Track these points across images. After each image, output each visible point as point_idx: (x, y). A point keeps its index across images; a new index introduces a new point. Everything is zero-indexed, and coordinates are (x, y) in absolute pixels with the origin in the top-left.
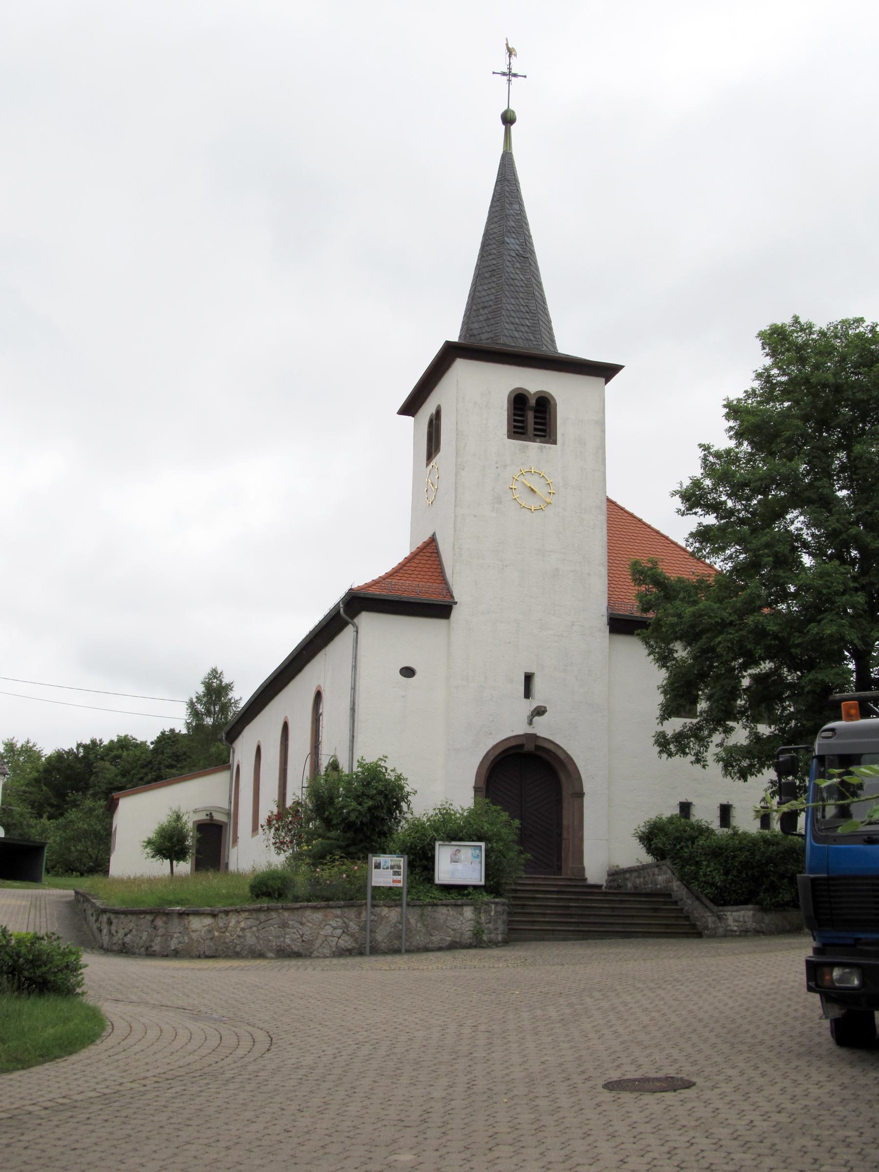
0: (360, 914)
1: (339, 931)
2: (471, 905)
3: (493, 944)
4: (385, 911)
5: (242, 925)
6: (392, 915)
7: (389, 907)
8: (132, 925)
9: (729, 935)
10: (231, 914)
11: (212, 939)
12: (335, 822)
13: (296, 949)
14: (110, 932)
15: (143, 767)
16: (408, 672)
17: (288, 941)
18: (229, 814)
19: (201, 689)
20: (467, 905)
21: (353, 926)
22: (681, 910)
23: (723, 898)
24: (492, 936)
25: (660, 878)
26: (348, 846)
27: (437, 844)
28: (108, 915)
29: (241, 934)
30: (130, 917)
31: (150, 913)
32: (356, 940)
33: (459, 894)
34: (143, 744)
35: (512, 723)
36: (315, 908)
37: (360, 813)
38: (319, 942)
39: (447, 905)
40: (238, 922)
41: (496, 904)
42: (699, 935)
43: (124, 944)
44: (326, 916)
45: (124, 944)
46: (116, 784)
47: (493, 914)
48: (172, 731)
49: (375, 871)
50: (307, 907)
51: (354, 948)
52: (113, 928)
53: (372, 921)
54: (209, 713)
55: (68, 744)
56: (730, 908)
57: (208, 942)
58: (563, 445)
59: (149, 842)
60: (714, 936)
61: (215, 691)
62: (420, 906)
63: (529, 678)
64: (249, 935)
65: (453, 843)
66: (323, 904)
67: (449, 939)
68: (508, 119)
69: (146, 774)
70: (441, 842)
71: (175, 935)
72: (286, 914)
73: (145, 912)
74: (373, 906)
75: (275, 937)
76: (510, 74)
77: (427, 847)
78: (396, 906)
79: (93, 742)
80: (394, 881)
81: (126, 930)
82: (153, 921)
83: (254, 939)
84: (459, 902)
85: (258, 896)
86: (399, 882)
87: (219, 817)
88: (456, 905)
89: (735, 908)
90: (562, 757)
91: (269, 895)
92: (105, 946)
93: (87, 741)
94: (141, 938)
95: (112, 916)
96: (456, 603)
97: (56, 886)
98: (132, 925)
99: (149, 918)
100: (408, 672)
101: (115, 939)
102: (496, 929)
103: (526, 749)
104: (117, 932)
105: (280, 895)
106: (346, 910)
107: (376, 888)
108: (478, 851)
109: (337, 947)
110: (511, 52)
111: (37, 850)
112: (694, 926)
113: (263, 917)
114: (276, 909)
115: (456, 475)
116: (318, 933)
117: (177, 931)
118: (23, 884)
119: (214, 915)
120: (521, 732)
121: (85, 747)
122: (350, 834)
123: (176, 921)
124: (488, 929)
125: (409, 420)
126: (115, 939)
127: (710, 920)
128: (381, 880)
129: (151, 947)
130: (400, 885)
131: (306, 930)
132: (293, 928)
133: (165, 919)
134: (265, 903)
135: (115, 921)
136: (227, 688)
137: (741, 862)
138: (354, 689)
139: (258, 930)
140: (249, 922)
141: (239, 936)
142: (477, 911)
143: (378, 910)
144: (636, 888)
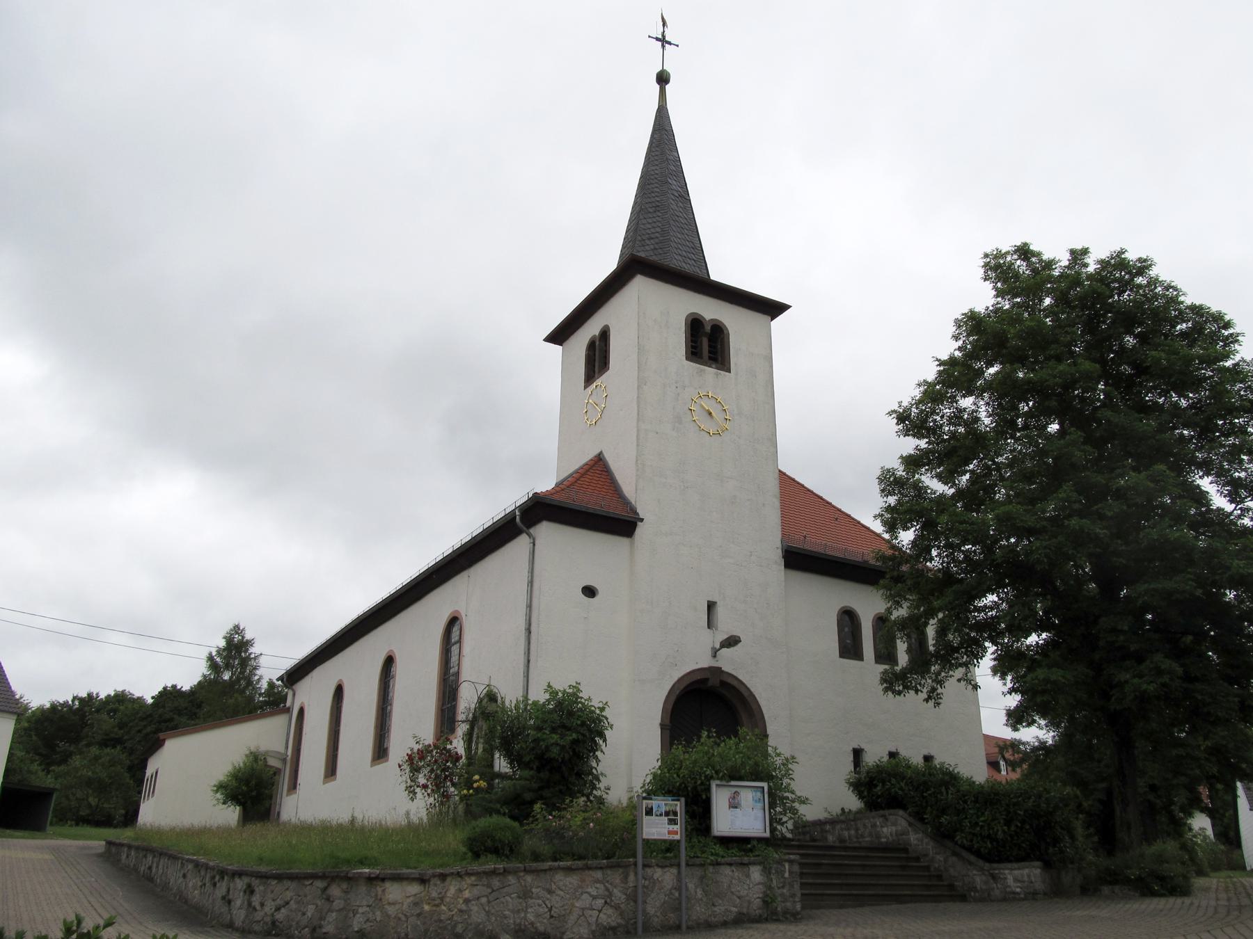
0: (626, 877)
1: (600, 902)
2: (760, 864)
3: (792, 917)
4: (658, 873)
5: (467, 894)
6: (666, 877)
7: (662, 867)
8: (289, 894)
9: (1009, 898)
10: (449, 879)
11: (419, 915)
12: (527, 759)
13: (541, 928)
14: (250, 904)
15: (142, 719)
16: (590, 592)
17: (531, 917)
18: (284, 761)
19: (222, 643)
20: (754, 864)
21: (619, 896)
22: (927, 868)
23: (998, 853)
24: (788, 904)
25: (885, 830)
26: (541, 788)
27: (714, 784)
28: (246, 880)
29: (464, 907)
30: (287, 883)
31: (323, 877)
32: (621, 914)
33: (740, 850)
34: (140, 700)
35: (696, 656)
36: (569, 870)
37: (563, 747)
38: (573, 918)
39: (731, 864)
40: (460, 891)
41: (791, 862)
42: (963, 898)
43: (274, 923)
44: (583, 881)
45: (274, 923)
46: (112, 735)
47: (787, 875)
48: (174, 687)
49: (646, 819)
50: (559, 868)
51: (619, 925)
52: (256, 900)
53: (644, 886)
54: (228, 666)
55: (64, 696)
56: (1009, 865)
57: (412, 920)
58: (737, 374)
59: (221, 787)
60: (986, 898)
61: (236, 650)
62: (702, 865)
63: (711, 606)
64: (475, 908)
65: (733, 783)
66: (580, 863)
67: (734, 909)
68: (663, 79)
69: (145, 726)
70: (718, 782)
71: (360, 910)
72: (529, 878)
73: (314, 877)
74: (645, 866)
75: (513, 911)
76: (663, 41)
77: (699, 788)
78: (671, 866)
79: (90, 695)
80: (670, 833)
81: (279, 902)
82: (325, 889)
83: (483, 914)
84: (746, 860)
85: (477, 855)
86: (676, 833)
87: (273, 762)
88: (742, 864)
89: (1015, 865)
90: (746, 694)
91: (496, 851)
92: (238, 923)
93: (84, 695)
94: (304, 914)
95: (255, 882)
96: (642, 520)
97: (75, 837)
98: (289, 894)
99: (320, 884)
100: (590, 592)
101: (258, 916)
102: (793, 896)
103: (710, 683)
104: (262, 905)
105: (511, 850)
106: (609, 872)
107: (647, 842)
108: (759, 794)
109: (597, 925)
110: (664, 24)
111: (43, 796)
112: (951, 887)
113: (496, 882)
114: (514, 872)
115: (639, 387)
116: (573, 905)
117: (365, 903)
118: (26, 833)
119: (423, 881)
120: (705, 665)
121: (81, 700)
122: (545, 775)
123: (363, 889)
124: (782, 895)
125: (558, 348)
126: (258, 916)
127: (979, 880)
128: (654, 830)
129: (321, 927)
130: (677, 837)
131: (555, 901)
132: (539, 898)
133: (345, 886)
134: (490, 863)
135: (259, 889)
136: (249, 643)
137: (1026, 811)
138: (530, 606)
139: (489, 902)
140: (476, 891)
141: (461, 911)
142: (767, 871)
143: (649, 870)
144: (842, 840)
